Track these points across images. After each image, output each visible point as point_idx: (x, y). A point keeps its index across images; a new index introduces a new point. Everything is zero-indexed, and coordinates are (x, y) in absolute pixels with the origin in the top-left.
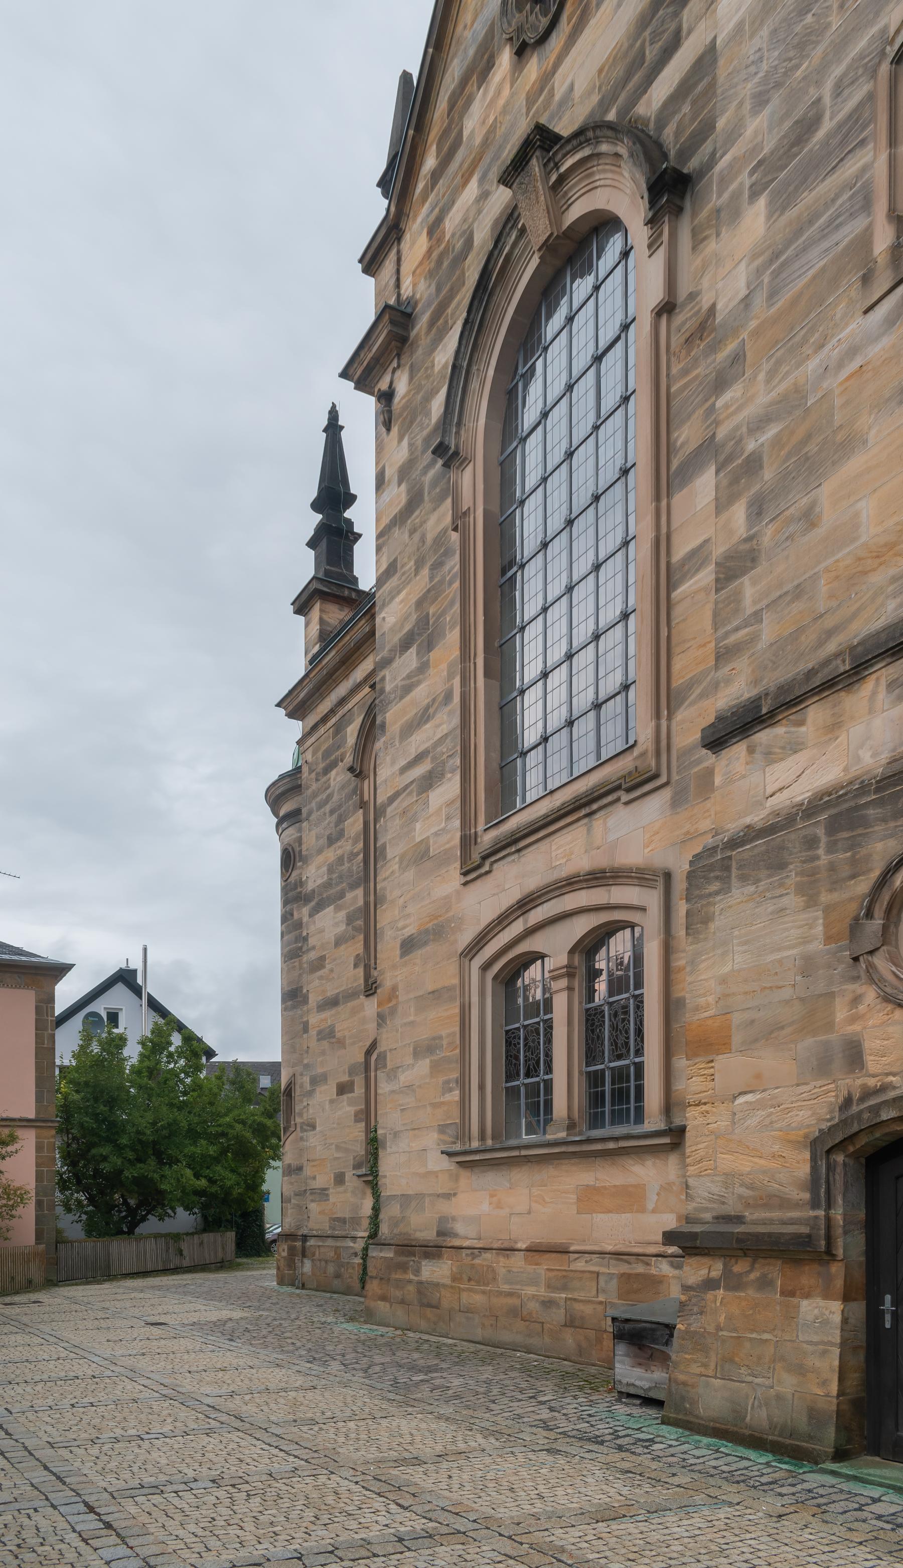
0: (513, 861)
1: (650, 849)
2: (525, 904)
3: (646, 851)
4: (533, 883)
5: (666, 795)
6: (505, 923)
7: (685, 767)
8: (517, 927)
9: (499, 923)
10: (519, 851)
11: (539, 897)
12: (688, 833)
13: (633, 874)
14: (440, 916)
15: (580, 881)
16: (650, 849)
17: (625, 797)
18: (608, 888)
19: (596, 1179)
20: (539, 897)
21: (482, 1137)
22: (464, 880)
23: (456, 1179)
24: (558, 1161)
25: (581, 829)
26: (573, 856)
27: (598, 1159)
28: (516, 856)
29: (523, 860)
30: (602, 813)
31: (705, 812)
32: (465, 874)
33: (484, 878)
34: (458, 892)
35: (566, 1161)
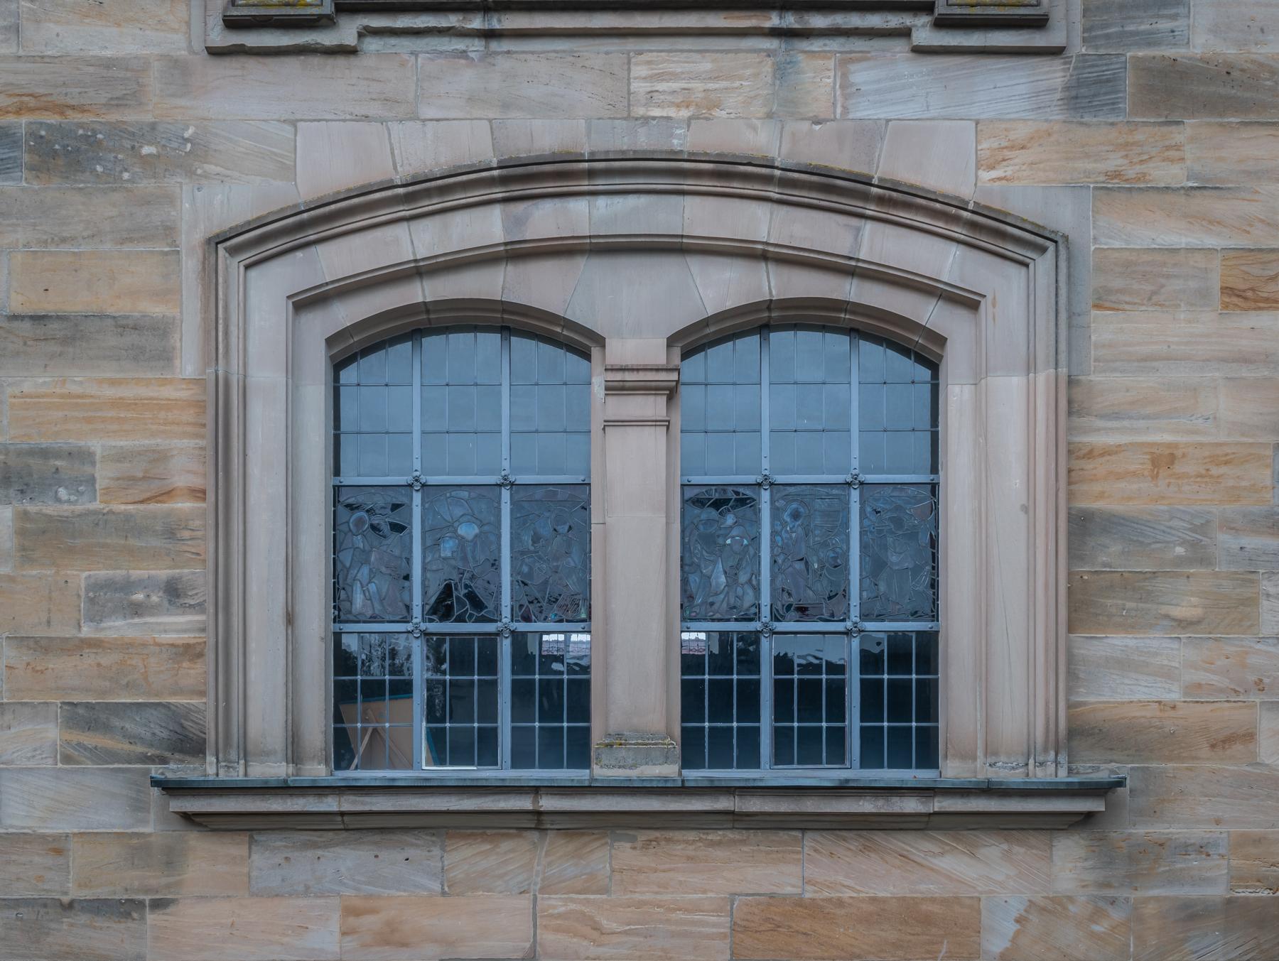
0: (463, 54)
1: (994, 174)
2: (523, 178)
3: (986, 175)
4: (544, 136)
5: (1053, 74)
6: (737, 187)
7: (1108, 36)
8: (487, 226)
9: (409, 198)
10: (489, 35)
11: (591, 174)
12: (1117, 175)
13: (965, 214)
14: (81, 109)
15: (768, 180)
16: (994, 174)
17: (924, 34)
18: (855, 222)
19: (806, 881)
20: (591, 174)
21: (295, 754)
22: (221, 38)
23: (171, 860)
24: (314, 837)
25: (753, 58)
26: (716, 112)
27: (809, 835)
28: (477, 45)
29: (503, 63)
30: (834, 44)
31: (1168, 148)
32: (232, 24)
33: (316, 60)
34: (177, 68)
35: (691, 835)
